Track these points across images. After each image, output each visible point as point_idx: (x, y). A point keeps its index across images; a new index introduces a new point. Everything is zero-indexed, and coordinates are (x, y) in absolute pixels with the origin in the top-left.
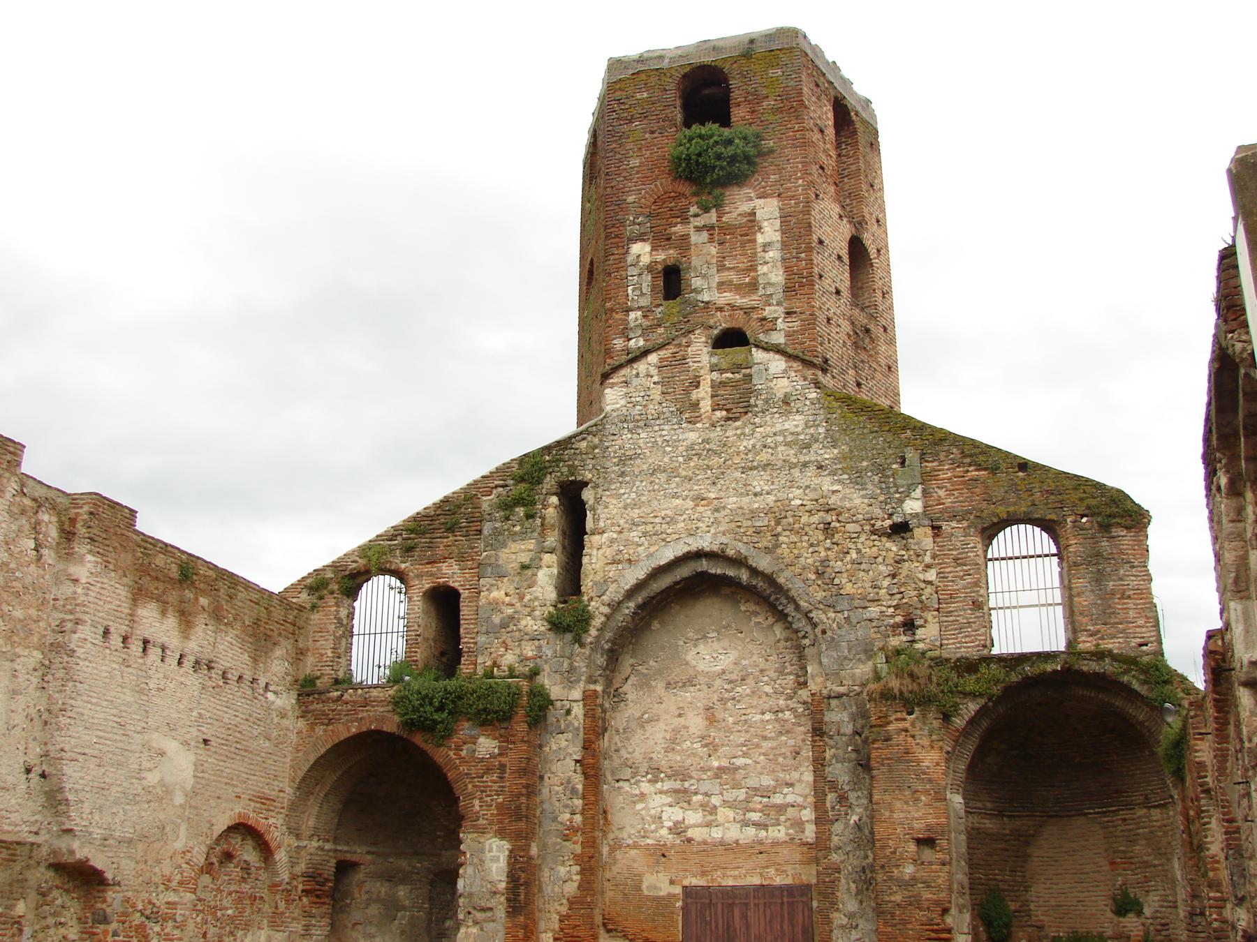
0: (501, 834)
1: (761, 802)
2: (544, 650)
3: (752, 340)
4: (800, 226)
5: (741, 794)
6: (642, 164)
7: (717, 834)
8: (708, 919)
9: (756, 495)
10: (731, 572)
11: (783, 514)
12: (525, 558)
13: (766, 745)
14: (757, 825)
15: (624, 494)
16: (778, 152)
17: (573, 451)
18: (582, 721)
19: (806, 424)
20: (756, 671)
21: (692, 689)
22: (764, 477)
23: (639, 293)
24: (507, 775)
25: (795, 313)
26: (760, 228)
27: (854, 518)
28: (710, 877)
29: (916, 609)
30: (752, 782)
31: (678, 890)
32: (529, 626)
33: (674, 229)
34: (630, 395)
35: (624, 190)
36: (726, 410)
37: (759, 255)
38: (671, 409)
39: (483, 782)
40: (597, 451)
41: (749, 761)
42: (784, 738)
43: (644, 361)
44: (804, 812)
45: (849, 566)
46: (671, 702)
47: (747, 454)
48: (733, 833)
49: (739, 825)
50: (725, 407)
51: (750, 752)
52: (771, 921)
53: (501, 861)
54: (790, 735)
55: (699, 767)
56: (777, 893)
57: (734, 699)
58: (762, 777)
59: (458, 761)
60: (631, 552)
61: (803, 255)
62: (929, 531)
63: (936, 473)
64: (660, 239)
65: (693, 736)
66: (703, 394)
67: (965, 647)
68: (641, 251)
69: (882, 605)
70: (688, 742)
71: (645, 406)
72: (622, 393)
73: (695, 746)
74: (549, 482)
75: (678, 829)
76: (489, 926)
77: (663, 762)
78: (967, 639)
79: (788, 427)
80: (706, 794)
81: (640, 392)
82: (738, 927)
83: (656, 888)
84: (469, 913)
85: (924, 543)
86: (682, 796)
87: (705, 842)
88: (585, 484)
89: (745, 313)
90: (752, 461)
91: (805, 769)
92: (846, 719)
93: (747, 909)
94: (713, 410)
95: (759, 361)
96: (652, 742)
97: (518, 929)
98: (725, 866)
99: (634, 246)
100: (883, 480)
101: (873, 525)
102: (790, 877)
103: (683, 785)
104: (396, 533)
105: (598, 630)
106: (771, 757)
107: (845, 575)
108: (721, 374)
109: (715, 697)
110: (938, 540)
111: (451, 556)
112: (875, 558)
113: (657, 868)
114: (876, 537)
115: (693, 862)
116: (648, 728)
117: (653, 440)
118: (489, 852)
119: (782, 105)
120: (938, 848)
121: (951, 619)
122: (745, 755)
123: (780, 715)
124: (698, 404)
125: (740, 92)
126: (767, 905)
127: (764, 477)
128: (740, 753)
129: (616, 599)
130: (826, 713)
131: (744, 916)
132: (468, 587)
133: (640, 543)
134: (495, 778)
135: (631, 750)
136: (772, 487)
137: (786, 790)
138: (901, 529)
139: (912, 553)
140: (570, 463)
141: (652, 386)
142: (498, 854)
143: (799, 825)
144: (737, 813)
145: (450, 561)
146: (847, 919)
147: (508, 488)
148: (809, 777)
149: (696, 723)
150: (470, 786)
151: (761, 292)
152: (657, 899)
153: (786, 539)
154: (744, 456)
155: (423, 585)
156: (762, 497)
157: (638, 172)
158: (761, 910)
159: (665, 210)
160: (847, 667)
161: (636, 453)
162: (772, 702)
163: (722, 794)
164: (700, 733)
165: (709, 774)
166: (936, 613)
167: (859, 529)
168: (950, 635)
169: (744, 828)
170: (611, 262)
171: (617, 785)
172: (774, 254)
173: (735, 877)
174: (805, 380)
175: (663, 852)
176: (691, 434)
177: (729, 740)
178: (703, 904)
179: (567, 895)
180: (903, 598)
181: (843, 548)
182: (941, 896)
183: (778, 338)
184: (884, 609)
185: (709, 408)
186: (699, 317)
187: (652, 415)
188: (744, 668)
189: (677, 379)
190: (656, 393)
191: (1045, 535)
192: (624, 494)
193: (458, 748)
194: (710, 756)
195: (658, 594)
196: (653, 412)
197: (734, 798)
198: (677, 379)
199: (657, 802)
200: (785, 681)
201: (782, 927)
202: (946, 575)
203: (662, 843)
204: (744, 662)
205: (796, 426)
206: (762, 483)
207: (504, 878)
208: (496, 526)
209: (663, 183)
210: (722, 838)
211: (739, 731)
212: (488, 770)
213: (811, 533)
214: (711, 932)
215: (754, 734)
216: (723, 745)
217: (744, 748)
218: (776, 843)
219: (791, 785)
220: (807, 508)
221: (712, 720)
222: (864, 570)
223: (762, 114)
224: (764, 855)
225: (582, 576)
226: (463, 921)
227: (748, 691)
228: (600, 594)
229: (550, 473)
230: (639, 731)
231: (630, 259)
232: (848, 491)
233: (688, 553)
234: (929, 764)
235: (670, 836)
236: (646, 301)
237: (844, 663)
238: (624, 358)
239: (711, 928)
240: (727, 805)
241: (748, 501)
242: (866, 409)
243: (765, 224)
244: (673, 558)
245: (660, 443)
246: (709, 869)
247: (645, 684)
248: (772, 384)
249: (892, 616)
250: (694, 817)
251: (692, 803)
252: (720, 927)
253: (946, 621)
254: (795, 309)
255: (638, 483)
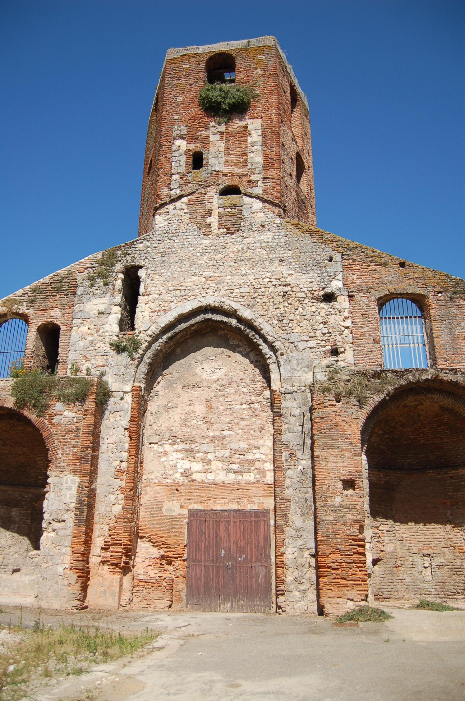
0: (74, 472)
1: (239, 458)
2: (109, 361)
3: (243, 192)
4: (273, 134)
5: (227, 453)
6: (184, 100)
7: (211, 477)
8: (204, 531)
9: (243, 275)
10: (225, 319)
11: (259, 286)
12: (102, 308)
13: (243, 423)
14: (236, 472)
15: (163, 273)
16: (262, 96)
17: (134, 249)
18: (130, 405)
19: (273, 237)
20: (238, 379)
21: (198, 389)
22: (248, 266)
23: (178, 165)
24: (80, 435)
25: (269, 178)
26: (250, 134)
27: (301, 290)
28: (205, 504)
29: (339, 342)
30: (233, 446)
31: (185, 512)
32: (101, 348)
33: (200, 133)
34: (170, 219)
35: (173, 113)
36: (226, 228)
37: (249, 148)
38: (194, 227)
39: (65, 439)
40: (149, 249)
41: (232, 433)
42: (254, 419)
43: (180, 201)
44: (266, 465)
45: (298, 317)
46: (185, 397)
47: (238, 253)
48: (221, 477)
49: (225, 472)
50: (226, 227)
51: (233, 427)
52: (243, 532)
53: (73, 489)
54: (257, 418)
55: (201, 436)
56: (248, 515)
57: (223, 396)
58: (240, 442)
59: (50, 426)
60: (166, 305)
61: (274, 149)
62: (347, 299)
63: (351, 266)
64: (192, 138)
65: (198, 417)
66: (213, 220)
67: (369, 366)
68: (182, 144)
69: (318, 340)
70: (195, 421)
71: (179, 225)
72: (165, 218)
73: (199, 423)
74: (119, 266)
75: (187, 474)
76: (62, 532)
77: (179, 432)
78: (371, 361)
79: (263, 238)
80: (205, 453)
81: (176, 217)
82: (223, 536)
83: (171, 510)
84: (50, 523)
85: (344, 304)
86: (190, 454)
87: (203, 482)
88: (141, 267)
89: (240, 178)
90: (241, 256)
91: (267, 438)
92: (295, 406)
93: (229, 525)
94: (219, 229)
95: (247, 203)
96: (173, 420)
97: (81, 534)
98: (215, 497)
99: (177, 141)
100: (319, 269)
101: (313, 294)
102: (257, 505)
103: (191, 446)
104: (24, 292)
105: (143, 351)
106: (246, 430)
107: (295, 322)
108: (224, 209)
109: (212, 395)
110: (352, 303)
111: (57, 306)
112: (314, 312)
113: (172, 498)
114: (314, 300)
115: (195, 494)
116: (171, 412)
117: (182, 243)
118: (66, 484)
119: (264, 73)
120: (356, 487)
121: (360, 348)
122: (230, 429)
123: (252, 405)
124: (210, 225)
125: (242, 66)
126: (242, 522)
127: (248, 266)
128: (227, 428)
129: (155, 332)
130: (283, 402)
131: (227, 529)
132: (65, 324)
133: (172, 301)
134: (72, 437)
135: (159, 425)
136: (253, 271)
137: (254, 451)
138: (329, 298)
139: (336, 310)
140: (133, 255)
141: (183, 214)
142: (71, 485)
143: (263, 473)
144: (224, 465)
145: (56, 309)
146: (295, 532)
147: (95, 269)
148: (270, 443)
149: (200, 409)
150: (56, 442)
151: (249, 167)
152: (172, 518)
153: (260, 301)
154: (236, 254)
155: (38, 322)
156: (246, 277)
157: (181, 104)
158: (238, 526)
159: (196, 123)
160: (296, 375)
161: (172, 251)
162: (248, 398)
163: (215, 453)
164: (202, 415)
165: (207, 440)
166: (351, 345)
167: (305, 296)
168: (360, 358)
169: (228, 474)
170: (163, 149)
171: (150, 446)
172: (258, 147)
173: (222, 504)
174: (273, 214)
175: (177, 488)
176: (205, 241)
177: (220, 420)
178: (201, 521)
179: (114, 513)
180: (331, 336)
181: (295, 306)
182: (358, 517)
183: (258, 191)
184: (319, 342)
185: (217, 227)
186: (213, 179)
187: (183, 230)
188: (231, 377)
189: (199, 211)
190: (186, 219)
191: (414, 305)
192: (163, 273)
193: (51, 418)
194: (208, 429)
195: (181, 331)
196: (183, 229)
197: (222, 455)
198: (199, 211)
199: (174, 457)
200: (256, 386)
201: (250, 537)
202: (357, 323)
203: (176, 482)
204: (231, 374)
205: (268, 238)
206: (246, 268)
207: (74, 500)
208: (86, 289)
209: (197, 110)
210: (214, 480)
211: (227, 415)
212: (69, 432)
213: (275, 297)
214: (206, 539)
215: (236, 416)
216: (216, 423)
217: (229, 425)
218: (248, 483)
219: (258, 448)
220: (273, 283)
221: (210, 408)
222: (307, 319)
223: (253, 77)
224: (240, 490)
225: (135, 319)
226: (46, 528)
227: (233, 391)
228: (145, 329)
229: (120, 261)
230: (164, 413)
231: (174, 148)
232: (297, 274)
233: (201, 307)
234: (351, 433)
235: (182, 478)
236: (182, 169)
237: (295, 373)
238: (168, 200)
239: (205, 536)
240: (218, 459)
241: (238, 278)
242: (309, 230)
243: (253, 132)
244: (191, 309)
245: (186, 246)
246: (205, 499)
247: (170, 386)
248: (254, 215)
249: (325, 346)
250: (197, 466)
251: (196, 457)
252: (211, 535)
253: (357, 350)
254: (269, 176)
255: (172, 267)
